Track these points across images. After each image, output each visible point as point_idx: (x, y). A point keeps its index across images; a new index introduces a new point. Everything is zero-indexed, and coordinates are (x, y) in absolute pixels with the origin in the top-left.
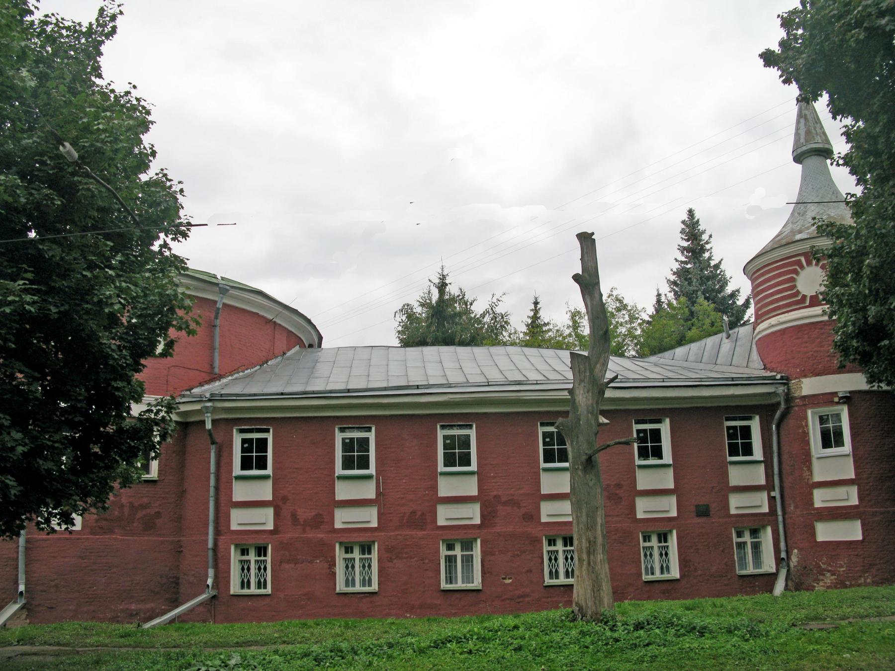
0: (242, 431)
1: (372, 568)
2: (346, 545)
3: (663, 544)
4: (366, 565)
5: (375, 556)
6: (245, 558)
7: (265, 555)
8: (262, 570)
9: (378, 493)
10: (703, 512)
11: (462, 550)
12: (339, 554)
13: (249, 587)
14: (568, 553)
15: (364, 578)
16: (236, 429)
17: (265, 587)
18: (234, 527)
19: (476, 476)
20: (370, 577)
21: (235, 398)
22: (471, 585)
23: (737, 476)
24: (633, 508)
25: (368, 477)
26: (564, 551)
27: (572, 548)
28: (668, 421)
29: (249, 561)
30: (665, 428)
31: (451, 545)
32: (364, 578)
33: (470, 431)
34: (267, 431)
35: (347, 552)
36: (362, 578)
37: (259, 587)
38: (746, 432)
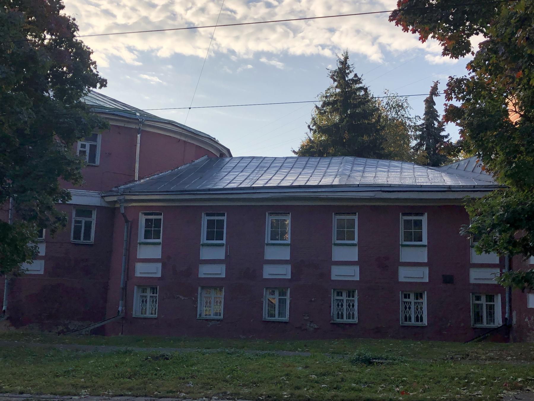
0: (146, 214)
1: (355, 307)
2: (338, 291)
3: (351, 298)
4: (351, 306)
5: (288, 297)
6: (145, 294)
7: (353, 297)
8: (408, 307)
9: (226, 256)
10: (448, 280)
11: (487, 301)
12: (334, 297)
13: (342, 318)
14: (418, 304)
15: (349, 314)
16: (204, 213)
17: (353, 318)
18: (138, 274)
19: (290, 247)
20: (421, 315)
21: (138, 194)
22: (273, 318)
23: (271, 253)
24: (395, 274)
25: (221, 245)
26: (415, 303)
27: (353, 299)
28: (426, 214)
29: (146, 297)
30: (424, 219)
31: (479, 296)
32: (349, 314)
33: (355, 216)
34: (161, 214)
35: (338, 295)
36: (348, 313)
37: (417, 321)
38: (419, 224)
